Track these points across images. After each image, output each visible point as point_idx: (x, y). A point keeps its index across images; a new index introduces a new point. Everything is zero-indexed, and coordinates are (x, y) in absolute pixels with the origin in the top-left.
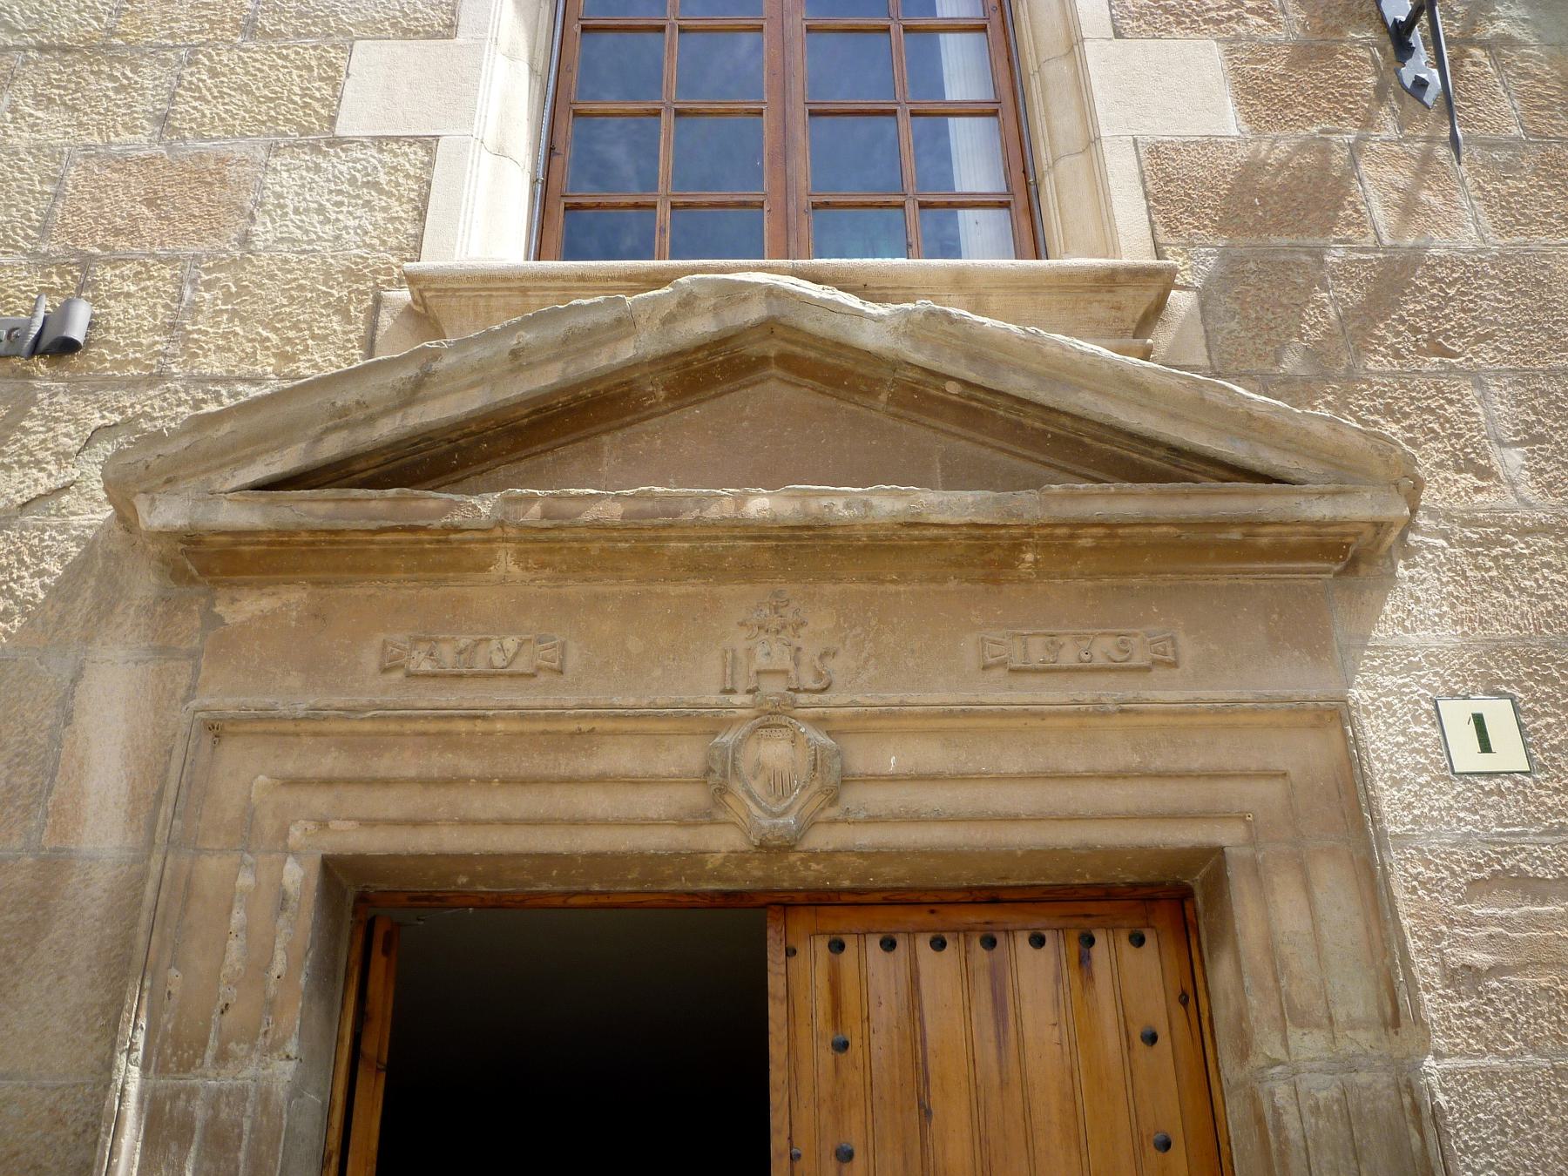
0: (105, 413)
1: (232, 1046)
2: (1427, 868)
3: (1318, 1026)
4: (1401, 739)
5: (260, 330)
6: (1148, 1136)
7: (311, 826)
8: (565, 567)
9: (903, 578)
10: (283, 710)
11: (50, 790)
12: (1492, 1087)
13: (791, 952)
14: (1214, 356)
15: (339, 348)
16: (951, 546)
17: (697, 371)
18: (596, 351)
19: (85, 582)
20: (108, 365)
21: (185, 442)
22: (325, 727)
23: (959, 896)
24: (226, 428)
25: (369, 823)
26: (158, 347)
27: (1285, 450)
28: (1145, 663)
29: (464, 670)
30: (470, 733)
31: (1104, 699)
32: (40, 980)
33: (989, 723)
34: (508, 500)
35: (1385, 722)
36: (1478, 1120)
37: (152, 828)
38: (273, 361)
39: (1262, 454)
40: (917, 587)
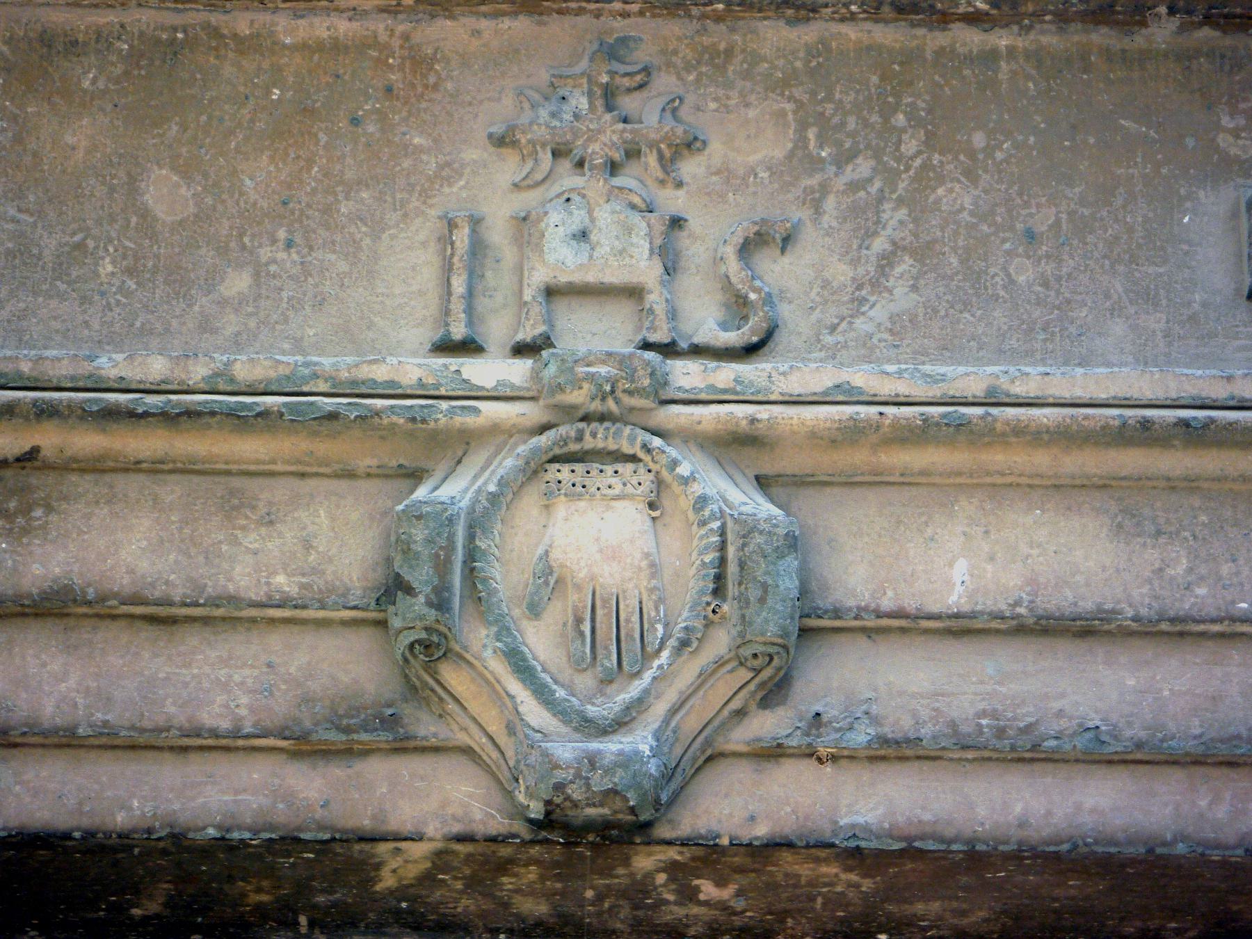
40: (1049, 38)
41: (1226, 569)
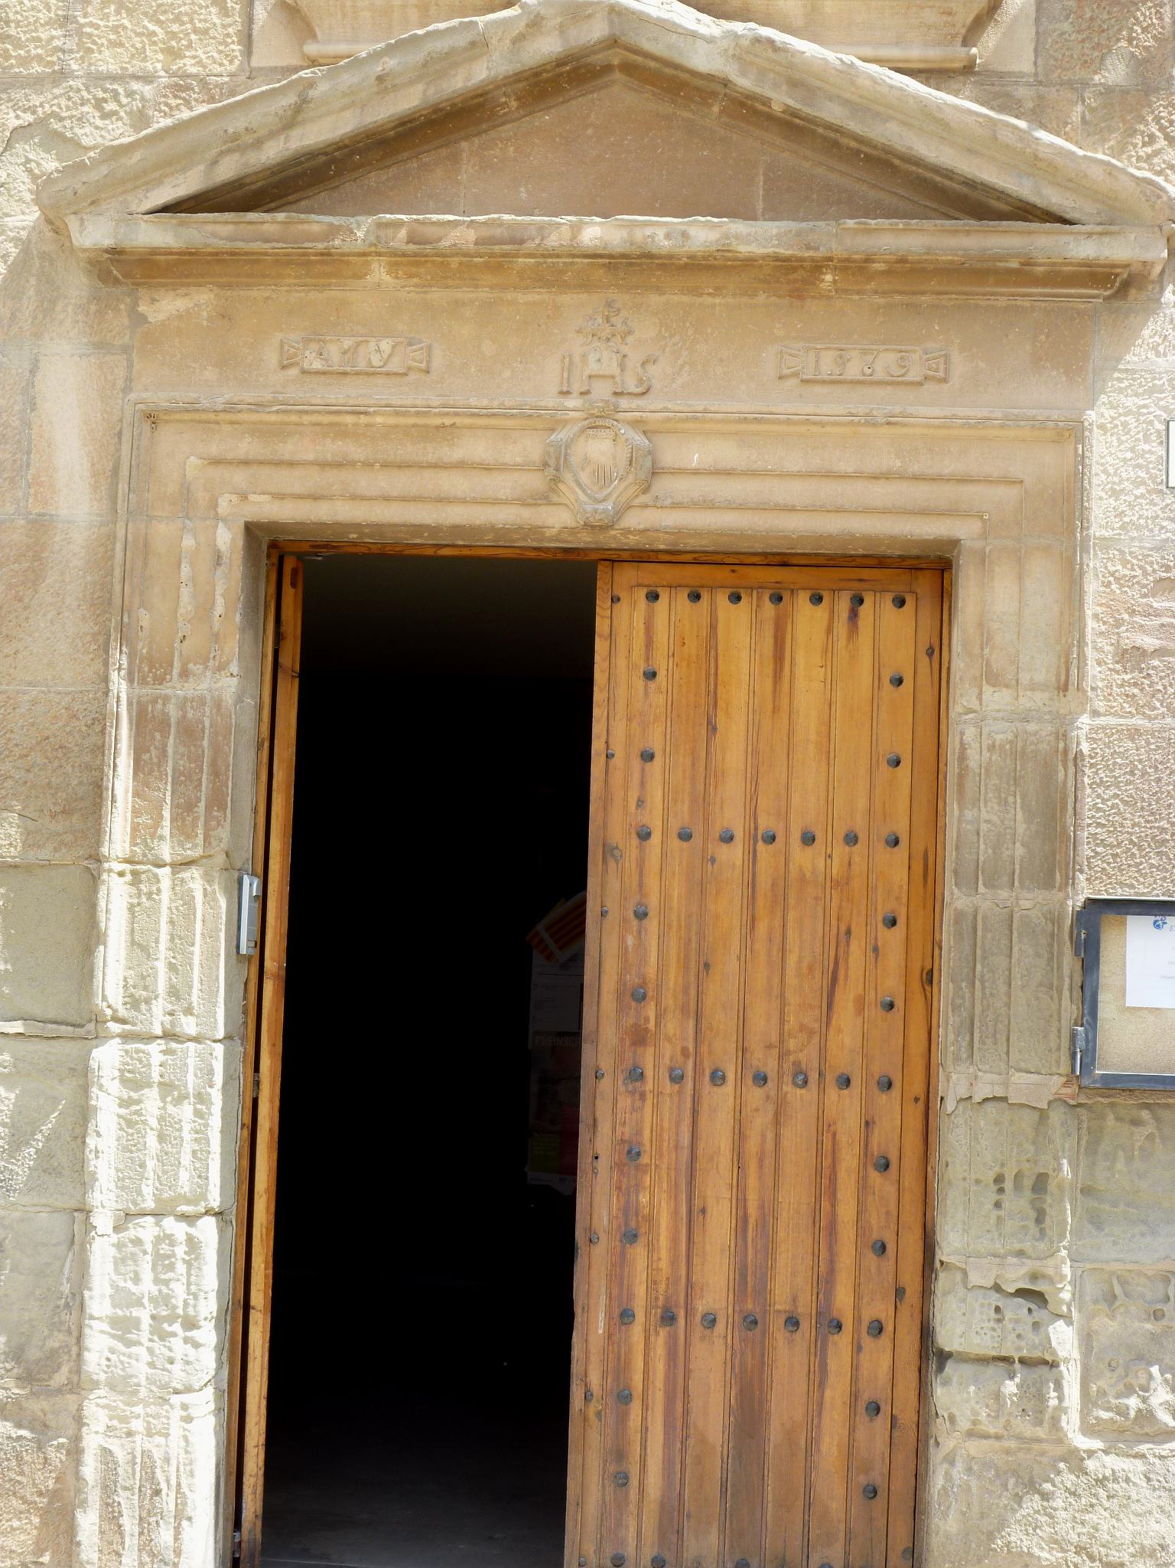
0: (19, 112)
1: (191, 666)
2: (1124, 567)
3: (1007, 686)
4: (1129, 455)
5: (146, 23)
6: (884, 756)
7: (235, 498)
8: (429, 277)
9: (718, 291)
10: (205, 403)
11: (28, 465)
12: (1133, 740)
13: (615, 600)
14: (1040, 62)
15: (220, 43)
16: (761, 266)
17: (546, 81)
18: (453, 72)
19: (28, 281)
20: (13, 61)
21: (104, 170)
22: (240, 417)
23: (755, 560)
24: (137, 156)
25: (280, 496)
26: (56, 43)
27: (1066, 188)
28: (918, 379)
29: (348, 369)
30: (356, 425)
31: (875, 413)
32: (44, 615)
33: (777, 428)
34: (380, 225)
35: (1119, 439)
36: (1115, 763)
37: (113, 499)
38: (160, 57)
39: (1044, 192)
40: (730, 300)
41: (766, 457)
